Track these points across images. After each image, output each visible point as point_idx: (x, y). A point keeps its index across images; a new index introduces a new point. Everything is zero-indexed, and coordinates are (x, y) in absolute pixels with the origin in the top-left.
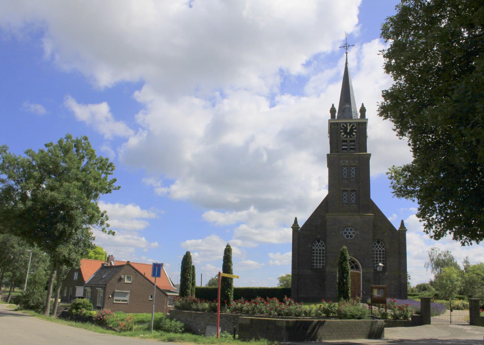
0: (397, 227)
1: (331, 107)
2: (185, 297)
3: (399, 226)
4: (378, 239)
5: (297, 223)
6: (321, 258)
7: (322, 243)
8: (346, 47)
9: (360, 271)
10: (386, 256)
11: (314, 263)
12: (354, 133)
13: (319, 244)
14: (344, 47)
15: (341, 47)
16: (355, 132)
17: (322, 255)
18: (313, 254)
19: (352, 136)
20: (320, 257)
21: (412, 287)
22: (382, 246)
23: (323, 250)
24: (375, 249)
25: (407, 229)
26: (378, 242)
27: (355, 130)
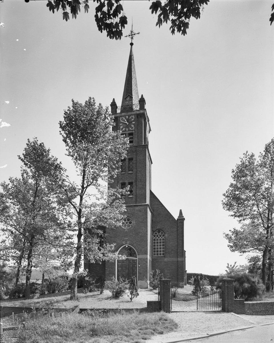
0: (176, 216)
1: (112, 102)
2: (191, 279)
3: (178, 215)
4: (159, 229)
5: (182, 215)
6: (159, 247)
7: (163, 233)
8: (133, 34)
9: (137, 258)
10: (165, 246)
11: (163, 251)
12: (133, 126)
13: (159, 234)
14: (134, 34)
15: (126, 36)
16: (133, 124)
17: (159, 244)
18: (164, 244)
19: (131, 129)
20: (158, 246)
21: (71, 274)
22: (162, 235)
23: (163, 240)
24: (156, 238)
25: (184, 217)
26: (159, 232)
27: (134, 123)
